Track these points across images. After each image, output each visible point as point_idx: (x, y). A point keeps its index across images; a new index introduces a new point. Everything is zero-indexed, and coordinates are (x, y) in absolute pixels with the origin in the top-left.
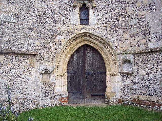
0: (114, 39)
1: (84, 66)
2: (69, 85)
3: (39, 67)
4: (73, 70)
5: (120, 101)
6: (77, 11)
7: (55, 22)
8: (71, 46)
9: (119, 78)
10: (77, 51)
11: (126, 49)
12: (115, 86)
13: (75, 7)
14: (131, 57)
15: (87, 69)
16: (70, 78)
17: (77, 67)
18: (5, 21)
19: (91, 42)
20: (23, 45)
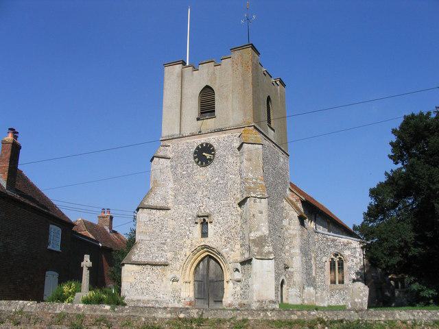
0: (228, 249)
1: (208, 275)
2: (196, 292)
3: (170, 275)
4: (200, 278)
5: (230, 305)
6: (199, 226)
7: (182, 236)
8: (195, 257)
9: (231, 284)
10: (202, 260)
11: (236, 258)
12: (231, 294)
13: (196, 223)
14: (239, 266)
15: (209, 285)
16: (196, 285)
17: (203, 275)
18: (142, 240)
19: (211, 253)
20: (157, 257)
